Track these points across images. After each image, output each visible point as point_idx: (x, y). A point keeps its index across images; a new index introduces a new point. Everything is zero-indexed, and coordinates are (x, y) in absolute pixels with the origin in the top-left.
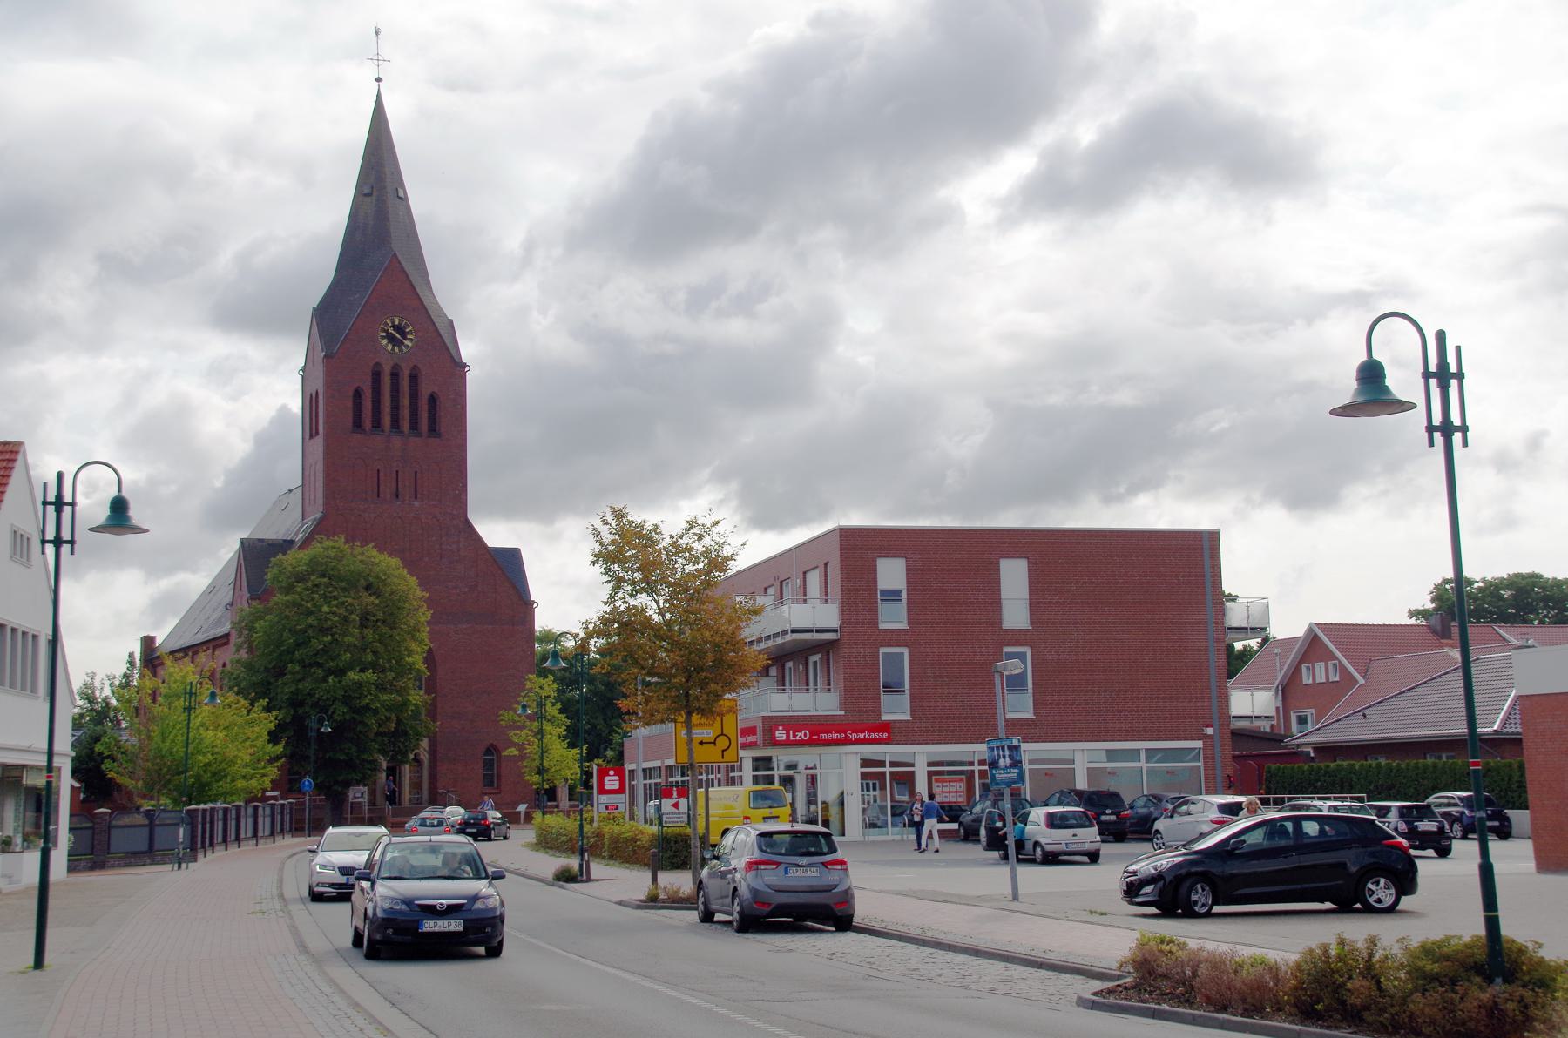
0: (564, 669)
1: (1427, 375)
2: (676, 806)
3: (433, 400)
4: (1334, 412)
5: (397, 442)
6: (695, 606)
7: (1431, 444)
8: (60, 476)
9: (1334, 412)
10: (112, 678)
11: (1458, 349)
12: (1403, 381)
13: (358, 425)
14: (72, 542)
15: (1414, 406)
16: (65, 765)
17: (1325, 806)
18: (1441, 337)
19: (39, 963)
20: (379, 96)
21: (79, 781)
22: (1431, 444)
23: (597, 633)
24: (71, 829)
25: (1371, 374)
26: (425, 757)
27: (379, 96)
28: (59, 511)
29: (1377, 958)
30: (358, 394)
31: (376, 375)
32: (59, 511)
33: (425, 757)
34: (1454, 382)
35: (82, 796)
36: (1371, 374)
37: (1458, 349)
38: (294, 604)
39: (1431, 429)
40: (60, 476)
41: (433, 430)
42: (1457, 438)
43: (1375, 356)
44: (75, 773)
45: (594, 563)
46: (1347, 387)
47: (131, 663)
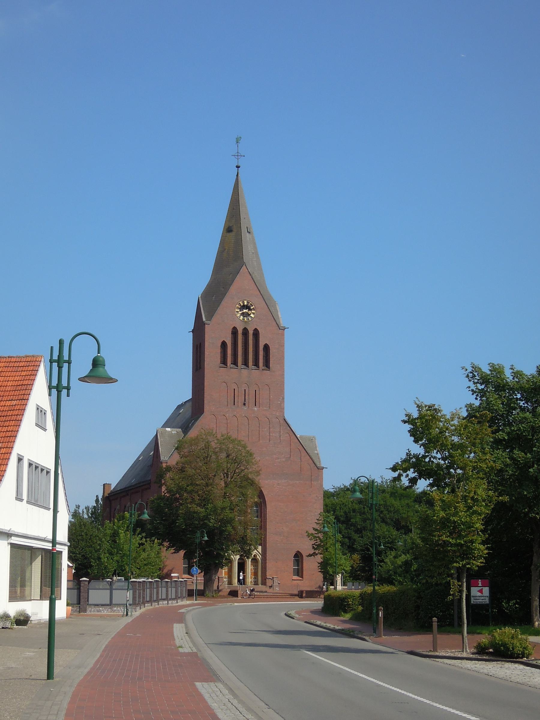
0: (360, 501)
2: (481, 591)
3: (267, 348)
5: (245, 372)
8: (61, 342)
10: (87, 508)
13: (224, 361)
14: (68, 388)
16: (63, 535)
19: (50, 675)
21: (72, 563)
24: (68, 589)
26: (259, 557)
28: (60, 368)
29: (475, 651)
30: (224, 345)
31: (235, 332)
32: (60, 368)
33: (259, 557)
35: (73, 571)
40: (61, 342)
41: (267, 364)
44: (70, 558)
45: (405, 422)
47: (97, 501)
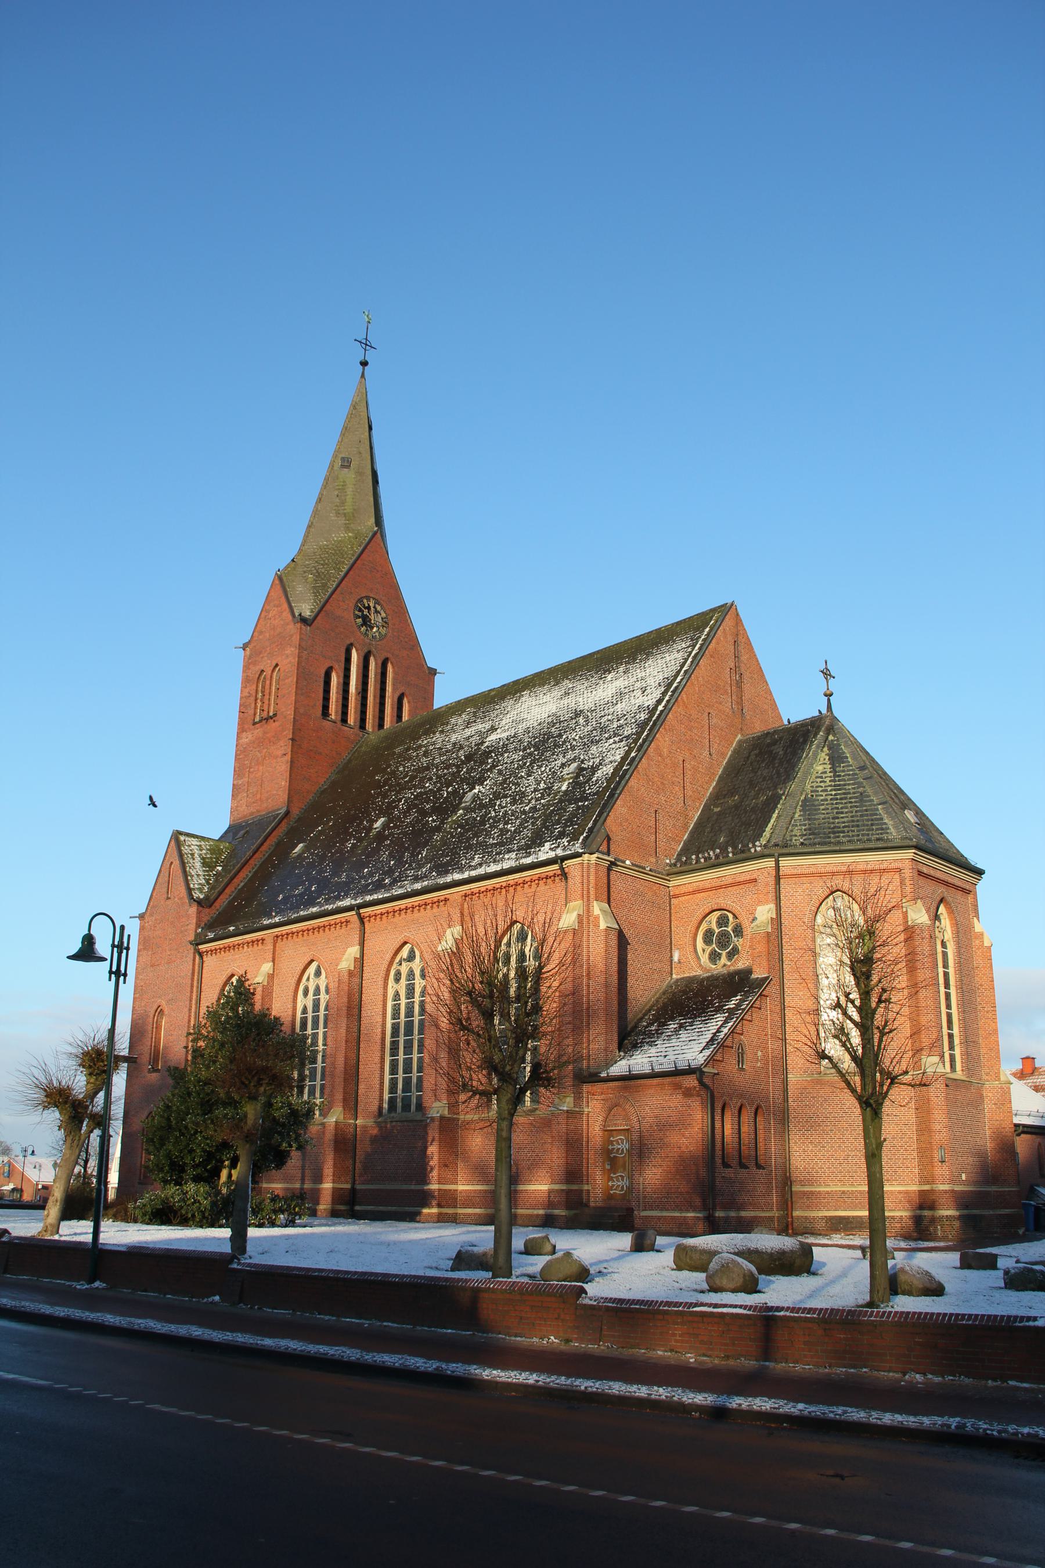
1: (113, 946)
4: (68, 957)
6: (493, 1042)
7: (110, 979)
9: (68, 957)
11: (129, 936)
12: (103, 947)
15: (106, 960)
17: (528, 1069)
18: (122, 928)
20: (361, 425)
22: (110, 979)
23: (650, 1035)
25: (89, 941)
27: (361, 425)
34: (125, 951)
36: (89, 941)
37: (129, 936)
38: (495, 784)
39: (111, 972)
42: (122, 978)
43: (92, 932)
46: (76, 946)
